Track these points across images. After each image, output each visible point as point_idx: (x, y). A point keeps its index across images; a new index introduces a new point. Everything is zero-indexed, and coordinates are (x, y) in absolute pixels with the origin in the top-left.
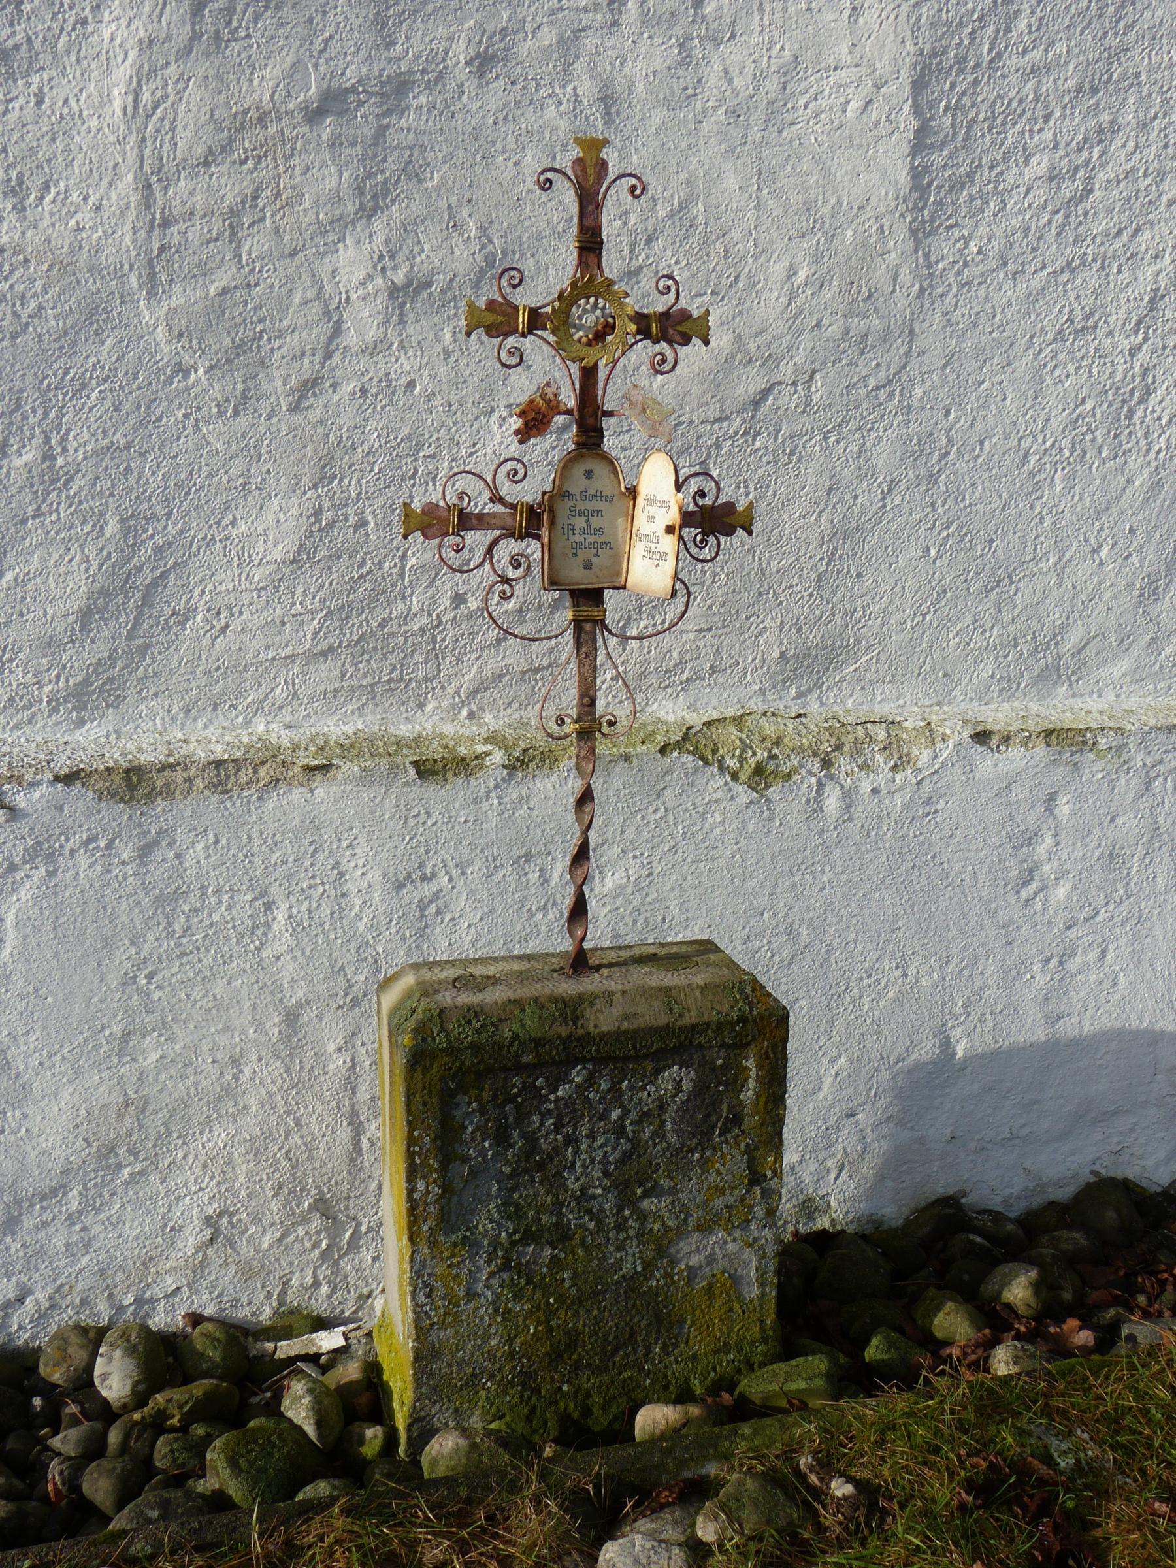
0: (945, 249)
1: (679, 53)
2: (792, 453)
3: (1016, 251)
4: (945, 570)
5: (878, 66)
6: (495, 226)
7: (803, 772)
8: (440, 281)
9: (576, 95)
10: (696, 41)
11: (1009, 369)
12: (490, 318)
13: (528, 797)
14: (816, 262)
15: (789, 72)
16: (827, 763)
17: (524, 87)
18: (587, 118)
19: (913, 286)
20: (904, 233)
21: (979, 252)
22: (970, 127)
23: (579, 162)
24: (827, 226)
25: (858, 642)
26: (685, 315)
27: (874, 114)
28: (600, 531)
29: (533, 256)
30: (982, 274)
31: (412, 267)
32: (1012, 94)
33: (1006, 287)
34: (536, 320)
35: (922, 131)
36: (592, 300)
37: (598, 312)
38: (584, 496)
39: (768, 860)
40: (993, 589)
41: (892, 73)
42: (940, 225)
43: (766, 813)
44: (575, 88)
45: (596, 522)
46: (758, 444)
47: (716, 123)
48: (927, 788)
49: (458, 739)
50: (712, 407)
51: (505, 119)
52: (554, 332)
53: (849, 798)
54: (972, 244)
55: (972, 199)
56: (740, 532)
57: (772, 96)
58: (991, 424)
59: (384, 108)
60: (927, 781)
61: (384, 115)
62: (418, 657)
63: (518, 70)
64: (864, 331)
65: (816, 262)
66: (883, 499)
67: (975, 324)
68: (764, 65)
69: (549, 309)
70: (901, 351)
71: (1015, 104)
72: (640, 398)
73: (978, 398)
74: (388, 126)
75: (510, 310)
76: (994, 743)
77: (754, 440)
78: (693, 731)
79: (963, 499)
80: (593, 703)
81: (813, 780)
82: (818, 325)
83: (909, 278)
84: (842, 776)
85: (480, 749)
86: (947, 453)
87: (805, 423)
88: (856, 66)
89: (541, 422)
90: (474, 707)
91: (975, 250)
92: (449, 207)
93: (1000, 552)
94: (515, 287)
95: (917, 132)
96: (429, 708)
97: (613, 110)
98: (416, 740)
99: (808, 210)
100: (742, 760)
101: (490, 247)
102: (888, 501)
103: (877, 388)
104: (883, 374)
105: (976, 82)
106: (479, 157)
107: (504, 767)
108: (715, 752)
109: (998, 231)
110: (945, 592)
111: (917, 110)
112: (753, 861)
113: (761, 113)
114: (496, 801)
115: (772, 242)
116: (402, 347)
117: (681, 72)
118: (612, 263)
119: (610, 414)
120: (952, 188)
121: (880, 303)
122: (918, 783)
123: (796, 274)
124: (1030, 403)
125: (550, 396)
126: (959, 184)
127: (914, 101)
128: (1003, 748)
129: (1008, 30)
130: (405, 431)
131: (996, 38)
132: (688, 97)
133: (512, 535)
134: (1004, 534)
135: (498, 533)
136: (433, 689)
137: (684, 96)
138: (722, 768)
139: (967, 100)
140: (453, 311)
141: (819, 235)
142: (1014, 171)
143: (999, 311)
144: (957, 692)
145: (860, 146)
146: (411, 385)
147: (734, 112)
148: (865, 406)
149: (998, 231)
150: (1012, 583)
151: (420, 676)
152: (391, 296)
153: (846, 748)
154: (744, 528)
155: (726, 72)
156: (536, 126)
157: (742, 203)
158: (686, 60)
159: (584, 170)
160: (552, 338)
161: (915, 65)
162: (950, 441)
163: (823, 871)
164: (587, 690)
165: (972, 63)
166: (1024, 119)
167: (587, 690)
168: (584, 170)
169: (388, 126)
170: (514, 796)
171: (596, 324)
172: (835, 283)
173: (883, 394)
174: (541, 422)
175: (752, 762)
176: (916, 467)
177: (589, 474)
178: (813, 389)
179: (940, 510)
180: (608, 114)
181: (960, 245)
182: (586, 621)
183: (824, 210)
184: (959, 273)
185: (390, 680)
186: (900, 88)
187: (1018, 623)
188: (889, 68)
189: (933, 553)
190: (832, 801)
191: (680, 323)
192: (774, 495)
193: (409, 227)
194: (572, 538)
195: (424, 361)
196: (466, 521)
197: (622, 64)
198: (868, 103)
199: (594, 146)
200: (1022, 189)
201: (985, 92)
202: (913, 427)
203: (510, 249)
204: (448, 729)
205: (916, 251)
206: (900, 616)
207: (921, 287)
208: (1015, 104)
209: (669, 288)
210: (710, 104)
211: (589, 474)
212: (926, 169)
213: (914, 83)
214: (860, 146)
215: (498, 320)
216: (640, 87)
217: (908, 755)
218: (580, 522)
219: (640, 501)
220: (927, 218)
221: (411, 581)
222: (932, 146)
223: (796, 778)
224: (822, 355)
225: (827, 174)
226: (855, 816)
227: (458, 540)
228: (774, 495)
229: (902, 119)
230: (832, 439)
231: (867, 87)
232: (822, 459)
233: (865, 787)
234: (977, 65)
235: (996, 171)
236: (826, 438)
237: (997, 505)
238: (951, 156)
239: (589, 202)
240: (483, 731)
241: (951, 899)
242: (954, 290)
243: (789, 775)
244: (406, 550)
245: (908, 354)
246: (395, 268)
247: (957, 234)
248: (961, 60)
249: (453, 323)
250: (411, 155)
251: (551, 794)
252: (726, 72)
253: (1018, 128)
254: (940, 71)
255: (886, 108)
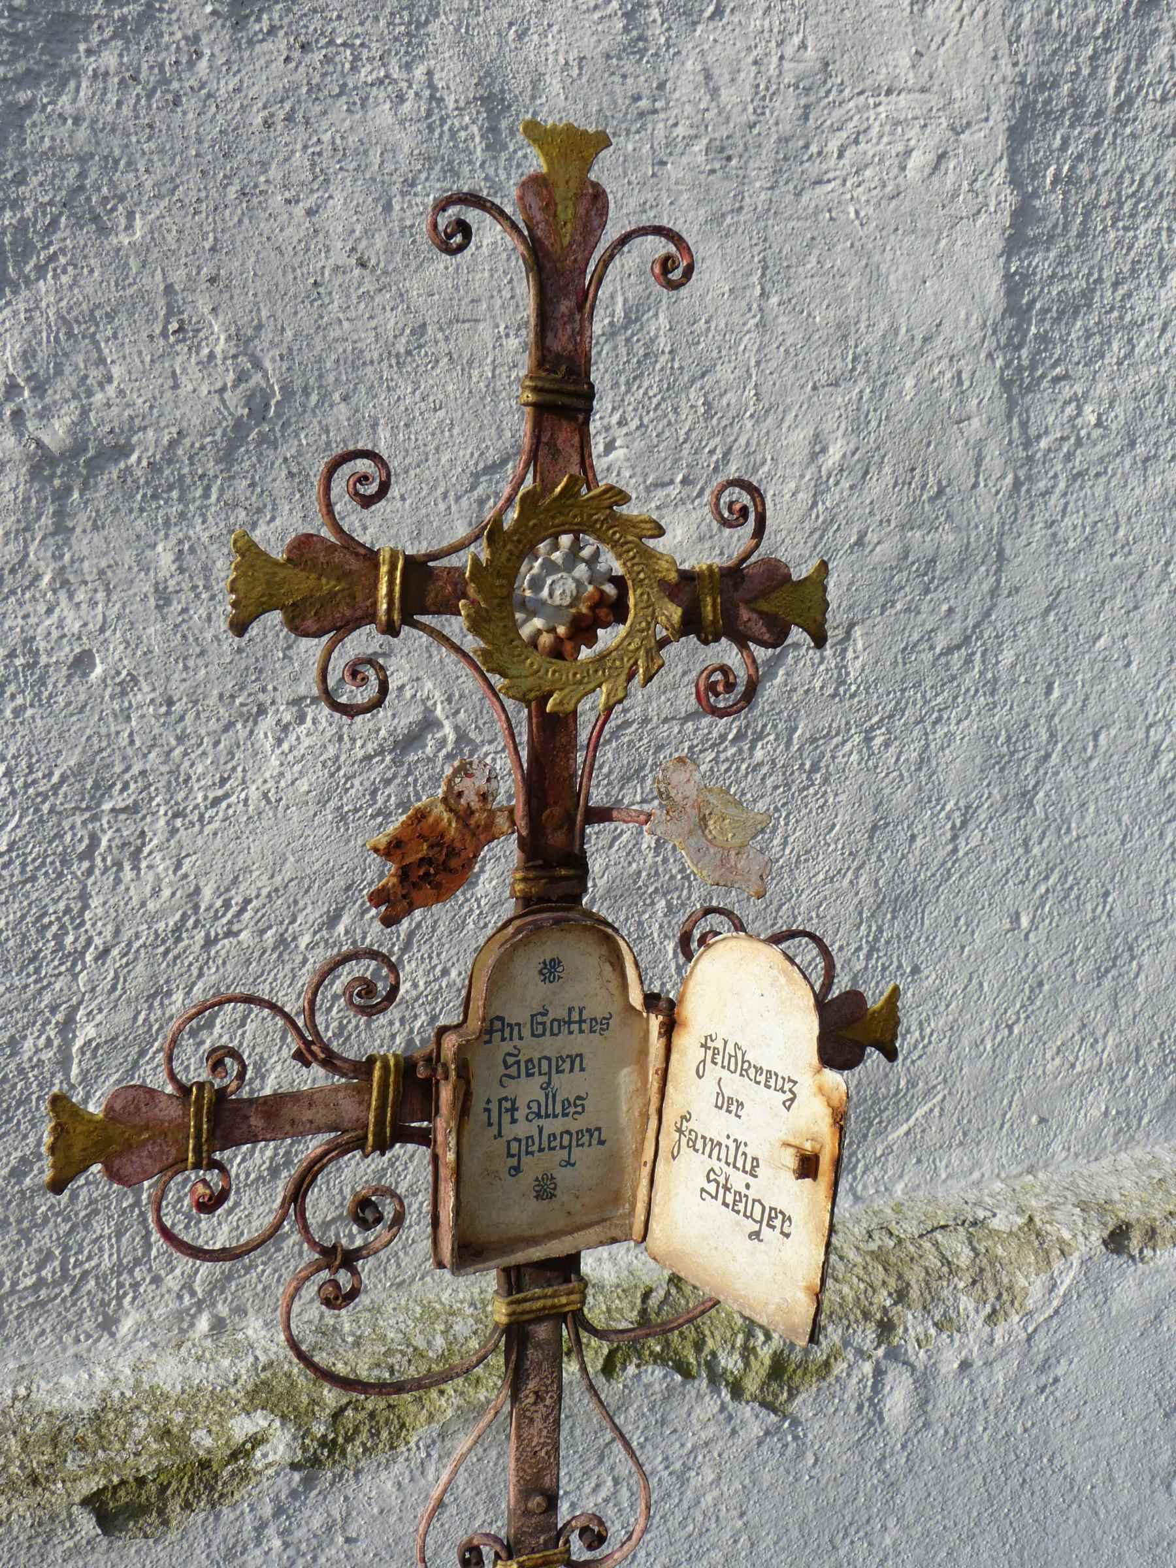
0: (1049, 415)
1: (626, 30)
2: (815, 768)
3: (1149, 423)
4: (1042, 948)
5: (957, 94)
6: (267, 335)
7: (850, 1354)
8: (147, 445)
9: (432, 86)
10: (655, 12)
11: (1136, 616)
12: (302, 584)
13: (345, 1520)
14: (856, 431)
15: (815, 86)
16: (886, 1328)
17: (327, 60)
18: (453, 134)
19: (1003, 477)
20: (992, 387)
21: (1099, 424)
22: (1086, 215)
23: (536, 184)
24: (874, 367)
25: (912, 1084)
26: (776, 576)
27: (950, 179)
28: (577, 1104)
29: (345, 398)
30: (1101, 460)
31: (85, 412)
32: (1146, 166)
33: (1133, 481)
34: (423, 588)
35: (1023, 214)
36: (565, 540)
37: (581, 570)
38: (542, 1025)
39: (795, 1533)
40: (1107, 971)
41: (978, 110)
42: (1043, 376)
43: (792, 1447)
44: (430, 73)
45: (567, 1085)
46: (759, 754)
47: (690, 167)
48: (1042, 1344)
49: (190, 1400)
50: (683, 692)
51: (289, 118)
52: (476, 626)
53: (924, 1385)
54: (1088, 409)
55: (1088, 335)
56: (874, 1056)
57: (786, 128)
58: (1110, 706)
59: (21, 67)
60: (1042, 1333)
61: (20, 81)
62: (101, 1227)
63: (316, 23)
64: (930, 553)
65: (856, 431)
66: (955, 837)
67: (1089, 542)
68: (773, 71)
69: (462, 560)
70: (985, 587)
71: (1149, 183)
72: (691, 790)
73: (1093, 662)
74: (29, 107)
75: (354, 564)
76: (1134, 1244)
77: (752, 749)
78: (654, 1301)
79: (1069, 830)
80: (551, 1501)
81: (868, 1368)
82: (860, 542)
83: (998, 463)
84: (912, 1346)
85: (242, 1427)
86: (1048, 756)
87: (832, 716)
88: (923, 90)
89: (445, 868)
90: (223, 1310)
91: (1093, 419)
92: (169, 289)
93: (1117, 912)
94: (367, 502)
95: (1015, 215)
96: (126, 1326)
97: (504, 124)
98: (97, 1418)
99: (845, 337)
100: (748, 1352)
101: (257, 377)
102: (961, 841)
103: (949, 651)
104: (957, 626)
105: (1096, 141)
106: (232, 191)
107: (294, 1466)
108: (699, 1346)
109: (1125, 389)
110: (1041, 984)
111: (1015, 178)
112: (769, 1540)
113: (765, 158)
114: (277, 1543)
115: (784, 391)
116: (62, 582)
117: (628, 66)
118: (617, 452)
119: (602, 815)
120: (1061, 313)
121: (954, 504)
122: (1030, 1338)
123: (824, 450)
124: (1164, 670)
125: (470, 798)
126: (1071, 308)
127: (1011, 161)
128: (1148, 1252)
129: (1142, 61)
130: (72, 760)
131: (1126, 71)
132: (641, 115)
133: (358, 1144)
134: (1124, 881)
135: (313, 1145)
136: (135, 1286)
137: (633, 113)
138: (715, 1378)
139: (1083, 169)
140: (177, 508)
141: (862, 383)
142: (1146, 292)
143: (1123, 521)
144: (1056, 1146)
145: (928, 232)
146: (82, 663)
147: (720, 150)
148: (929, 682)
149: (1125, 389)
150: (1133, 958)
151: (106, 1264)
152: (35, 473)
153: (914, 1293)
154: (880, 1047)
155: (708, 77)
156: (352, 140)
157: (736, 318)
158: (637, 46)
159: (549, 206)
160: (471, 643)
161: (1013, 99)
162: (1052, 735)
163: (884, 1528)
164: (538, 1476)
165: (1092, 109)
166: (1161, 208)
167: (538, 1476)
168: (549, 206)
169: (29, 107)
170: (316, 1524)
171: (576, 600)
172: (887, 469)
173: (957, 658)
174: (445, 868)
175: (765, 1354)
176: (1003, 781)
177: (551, 970)
178: (850, 654)
179: (1036, 851)
180: (494, 129)
181: (1070, 409)
182: (539, 1320)
183: (869, 339)
184: (1069, 457)
185: (40, 1283)
186: (989, 137)
187: (1142, 1024)
188: (973, 100)
189: (1025, 921)
190: (898, 1398)
191: (764, 594)
192: (785, 844)
193: (78, 328)
194: (510, 1131)
195: (113, 612)
196: (225, 1117)
197: (520, 36)
198: (942, 157)
199: (575, 147)
200: (1157, 323)
201: (1110, 160)
202: (1001, 713)
203: (298, 383)
204: (169, 1373)
205: (1009, 418)
206: (973, 1033)
207: (1016, 478)
208: (1149, 183)
209: (744, 511)
210: (680, 131)
211: (551, 970)
212: (1026, 278)
213: (1012, 131)
214: (928, 232)
215: (319, 589)
216: (554, 84)
217: (1010, 1289)
218: (528, 1090)
219: (688, 1044)
220: (1025, 363)
221: (84, 1074)
222: (1035, 242)
223: (839, 1368)
224: (865, 594)
225: (874, 276)
226: (934, 1417)
227: (213, 1176)
228: (785, 844)
229: (992, 190)
230: (878, 741)
231: (940, 128)
232: (861, 777)
233: (949, 1363)
234: (1099, 113)
235: (1121, 291)
236: (868, 740)
237: (1115, 835)
238: (1062, 260)
239: (560, 281)
240: (243, 1366)
241: (1076, 1523)
242: (1062, 485)
243: (827, 1364)
244: (74, 1009)
245: (994, 592)
246: (45, 414)
247: (1067, 393)
248: (1078, 101)
249: (176, 533)
250: (82, 175)
251: (394, 1501)
252: (708, 77)
253: (1152, 223)
254: (1048, 114)
255: (969, 170)
